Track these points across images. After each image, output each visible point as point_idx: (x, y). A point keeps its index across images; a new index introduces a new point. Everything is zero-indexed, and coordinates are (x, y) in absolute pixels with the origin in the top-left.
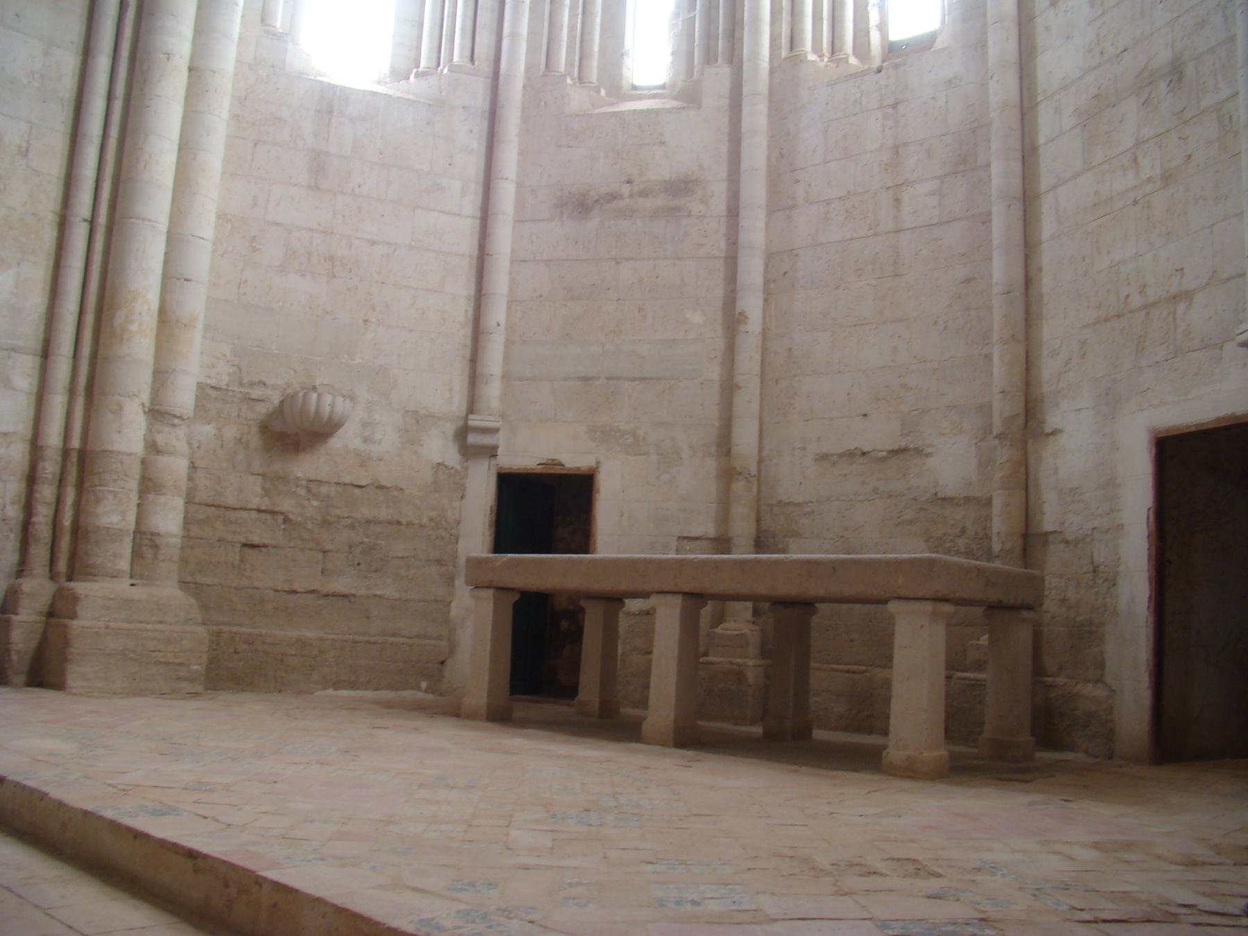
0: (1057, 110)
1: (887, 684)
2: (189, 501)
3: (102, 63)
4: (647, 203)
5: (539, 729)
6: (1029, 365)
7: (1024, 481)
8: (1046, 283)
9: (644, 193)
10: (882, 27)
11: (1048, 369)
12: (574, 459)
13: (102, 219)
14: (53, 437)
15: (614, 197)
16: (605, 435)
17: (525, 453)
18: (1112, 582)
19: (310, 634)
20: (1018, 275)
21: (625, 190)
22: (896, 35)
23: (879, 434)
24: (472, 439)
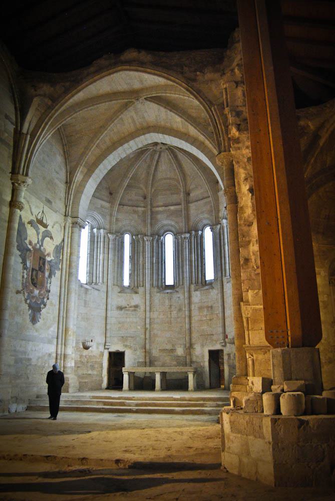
0: (195, 306)
1: (327, 398)
2: (75, 361)
3: (63, 289)
4: (131, 309)
5: (165, 392)
6: (190, 339)
7: (190, 354)
8: (193, 329)
9: (131, 307)
10: (165, 282)
11: (193, 341)
12: (121, 349)
13: (65, 316)
14: (59, 352)
15: (126, 307)
16: (126, 346)
17: (113, 349)
18: (204, 368)
19: (86, 381)
20: (189, 327)
21: (128, 306)
22: (167, 284)
23: (169, 347)
24: (106, 347)
